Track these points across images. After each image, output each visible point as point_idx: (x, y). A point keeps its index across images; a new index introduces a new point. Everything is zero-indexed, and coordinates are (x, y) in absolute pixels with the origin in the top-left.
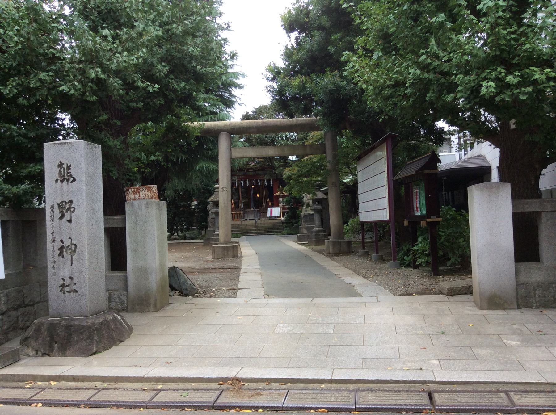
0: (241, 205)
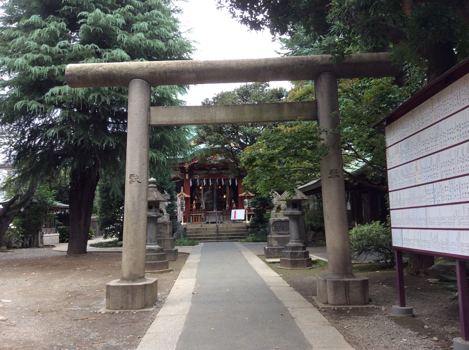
0: (203, 206)
